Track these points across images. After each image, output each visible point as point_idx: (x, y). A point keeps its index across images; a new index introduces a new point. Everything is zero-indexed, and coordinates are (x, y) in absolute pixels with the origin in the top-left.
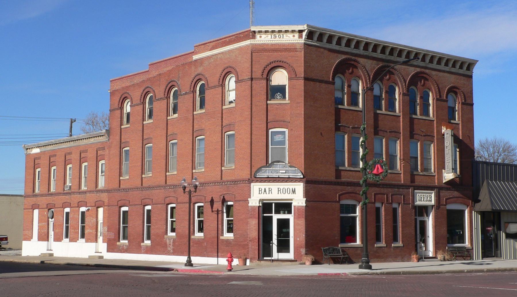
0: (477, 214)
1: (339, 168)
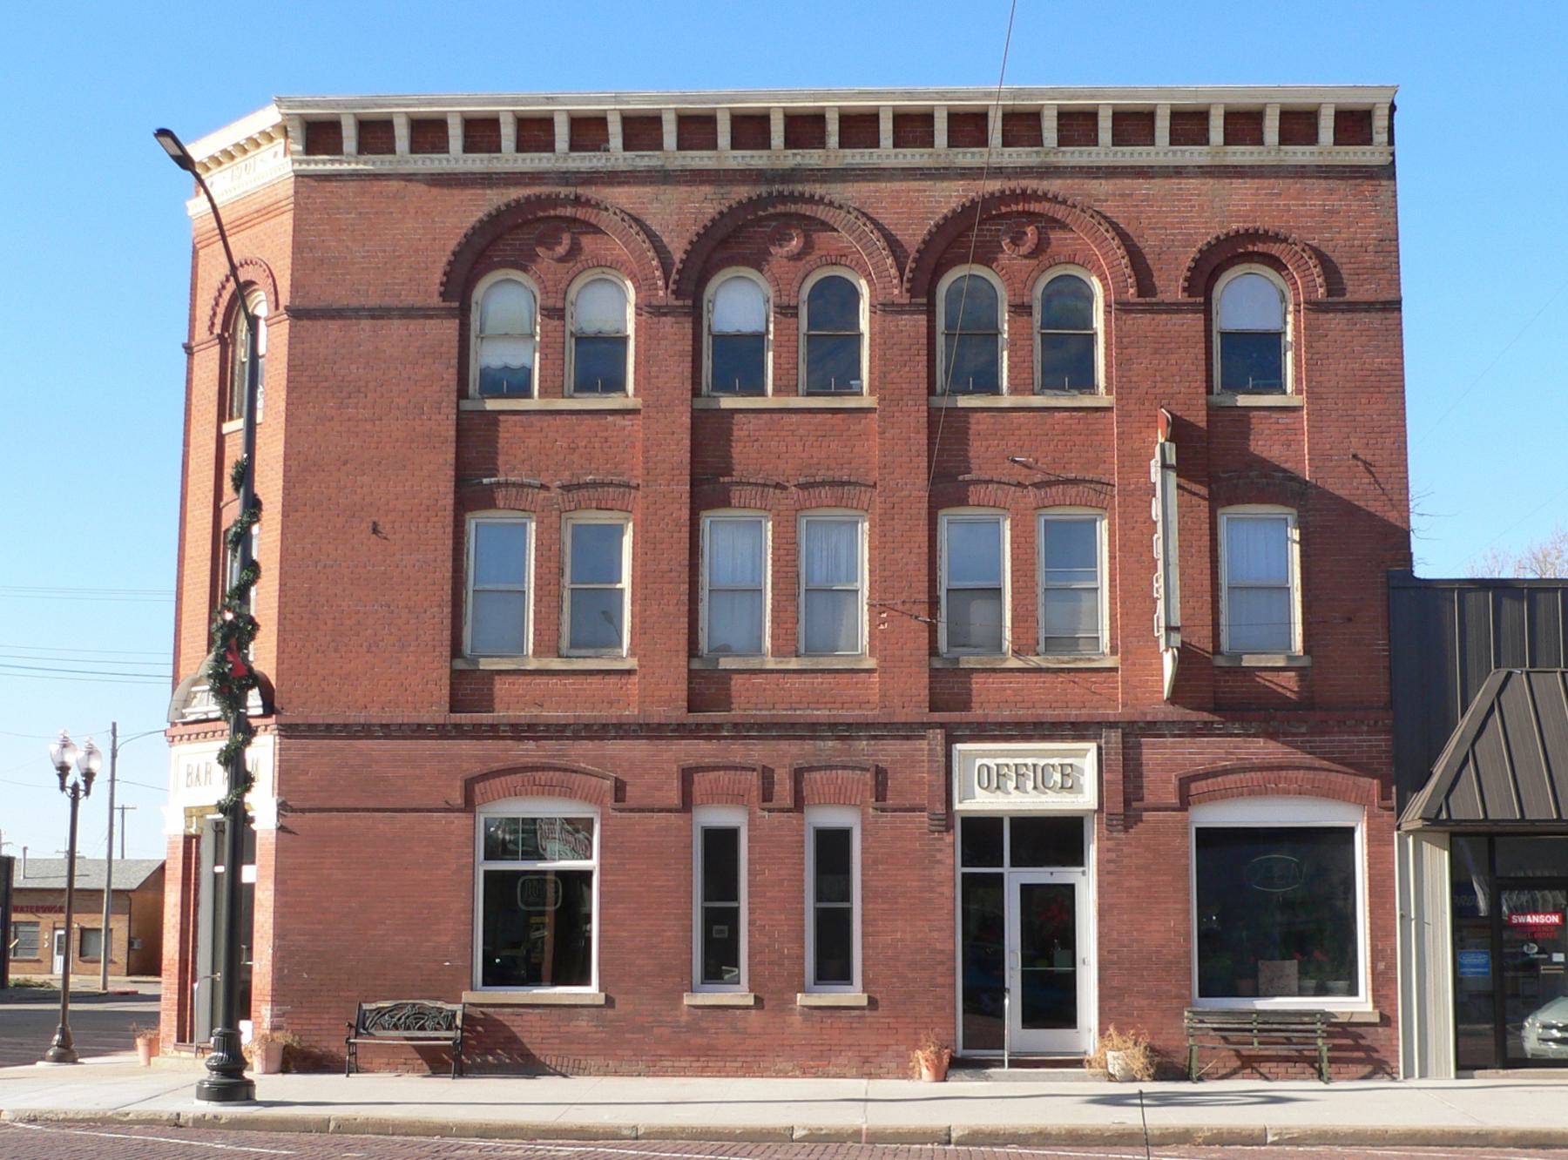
0: (1427, 847)
1: (477, 663)
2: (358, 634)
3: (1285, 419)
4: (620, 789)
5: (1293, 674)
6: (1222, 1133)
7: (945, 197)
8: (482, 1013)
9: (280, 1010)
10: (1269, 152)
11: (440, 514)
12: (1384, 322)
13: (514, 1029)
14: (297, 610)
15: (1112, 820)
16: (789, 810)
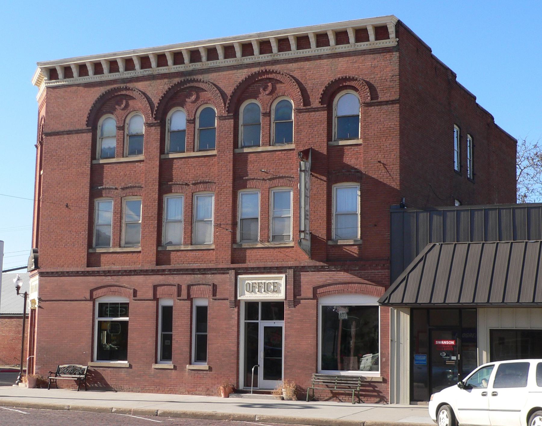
1: (96, 250)
2: (62, 241)
3: (356, 149)
4: (135, 293)
5: (356, 247)
6: (241, 417)
7: (241, 75)
8: (94, 369)
9: (38, 367)
10: (351, 46)
11: (85, 200)
12: (393, 108)
13: (103, 375)
14: (45, 234)
15: (289, 303)
16: (186, 300)
